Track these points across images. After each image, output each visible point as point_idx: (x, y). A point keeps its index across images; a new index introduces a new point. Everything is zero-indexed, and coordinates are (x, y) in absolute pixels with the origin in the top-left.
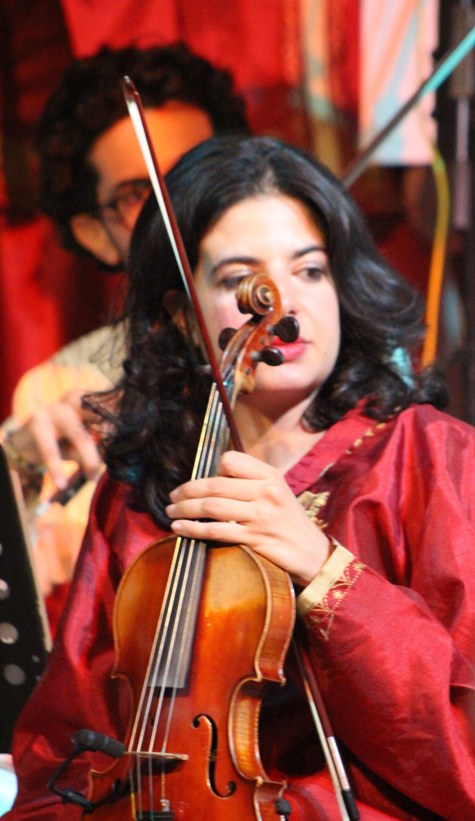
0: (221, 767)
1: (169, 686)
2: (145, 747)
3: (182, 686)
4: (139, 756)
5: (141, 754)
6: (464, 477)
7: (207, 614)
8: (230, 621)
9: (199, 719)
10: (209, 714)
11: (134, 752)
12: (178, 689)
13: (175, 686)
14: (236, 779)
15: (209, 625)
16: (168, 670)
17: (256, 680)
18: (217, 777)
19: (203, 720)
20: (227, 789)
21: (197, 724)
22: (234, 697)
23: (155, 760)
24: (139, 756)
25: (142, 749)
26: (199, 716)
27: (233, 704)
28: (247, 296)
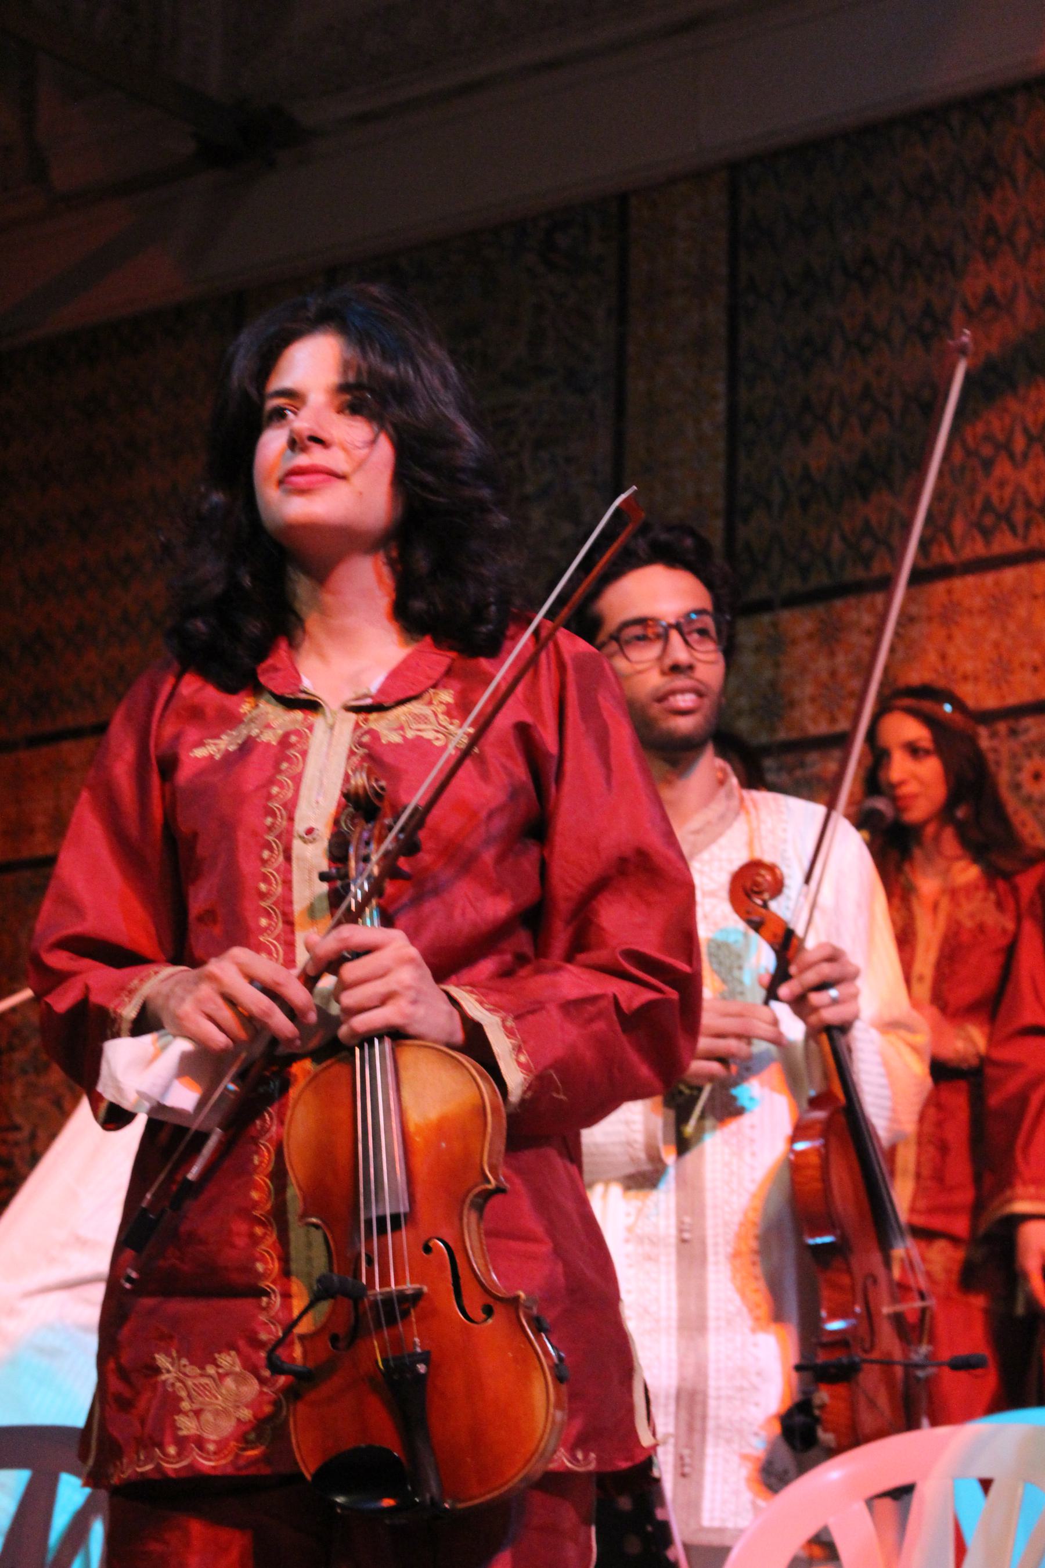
0: (469, 1288)
1: (395, 1211)
2: (385, 1281)
3: (408, 1209)
4: (379, 1298)
5: (381, 1294)
6: (289, 1113)
7: (412, 1128)
8: (441, 1128)
9: (431, 1244)
10: (440, 1237)
11: (387, 1289)
12: (405, 1214)
13: (402, 1210)
14: (490, 1301)
15: (417, 1139)
16: (390, 1195)
17: (489, 1187)
18: (466, 1302)
19: (437, 1244)
20: (480, 1315)
21: (427, 1249)
22: (465, 1212)
23: (402, 1297)
24: (379, 1298)
25: (396, 1284)
26: (430, 1239)
27: (465, 1220)
28: (364, 788)
